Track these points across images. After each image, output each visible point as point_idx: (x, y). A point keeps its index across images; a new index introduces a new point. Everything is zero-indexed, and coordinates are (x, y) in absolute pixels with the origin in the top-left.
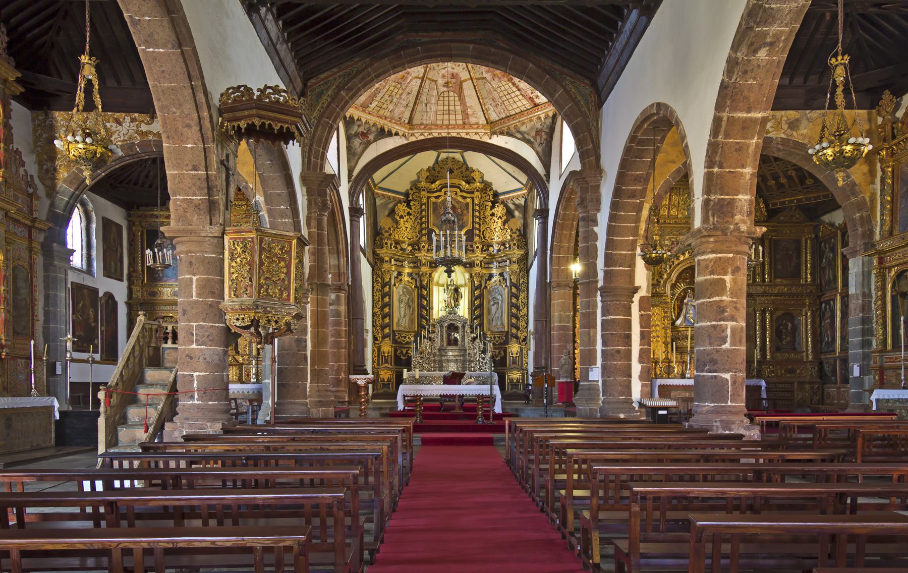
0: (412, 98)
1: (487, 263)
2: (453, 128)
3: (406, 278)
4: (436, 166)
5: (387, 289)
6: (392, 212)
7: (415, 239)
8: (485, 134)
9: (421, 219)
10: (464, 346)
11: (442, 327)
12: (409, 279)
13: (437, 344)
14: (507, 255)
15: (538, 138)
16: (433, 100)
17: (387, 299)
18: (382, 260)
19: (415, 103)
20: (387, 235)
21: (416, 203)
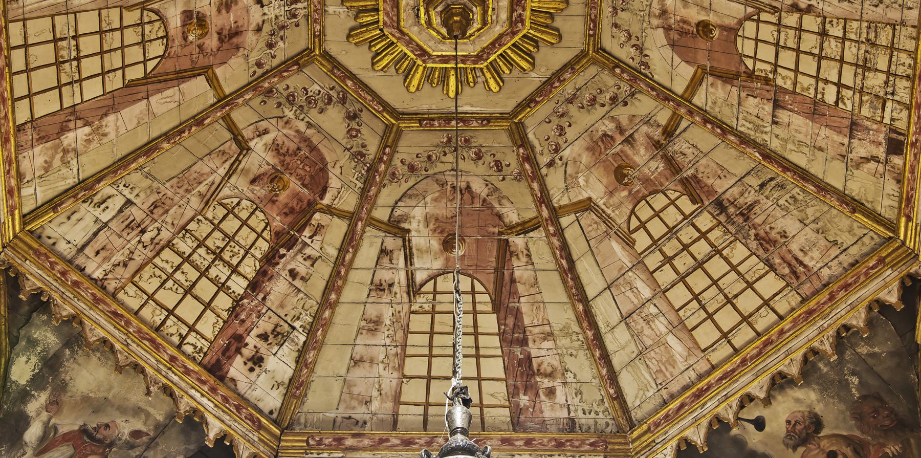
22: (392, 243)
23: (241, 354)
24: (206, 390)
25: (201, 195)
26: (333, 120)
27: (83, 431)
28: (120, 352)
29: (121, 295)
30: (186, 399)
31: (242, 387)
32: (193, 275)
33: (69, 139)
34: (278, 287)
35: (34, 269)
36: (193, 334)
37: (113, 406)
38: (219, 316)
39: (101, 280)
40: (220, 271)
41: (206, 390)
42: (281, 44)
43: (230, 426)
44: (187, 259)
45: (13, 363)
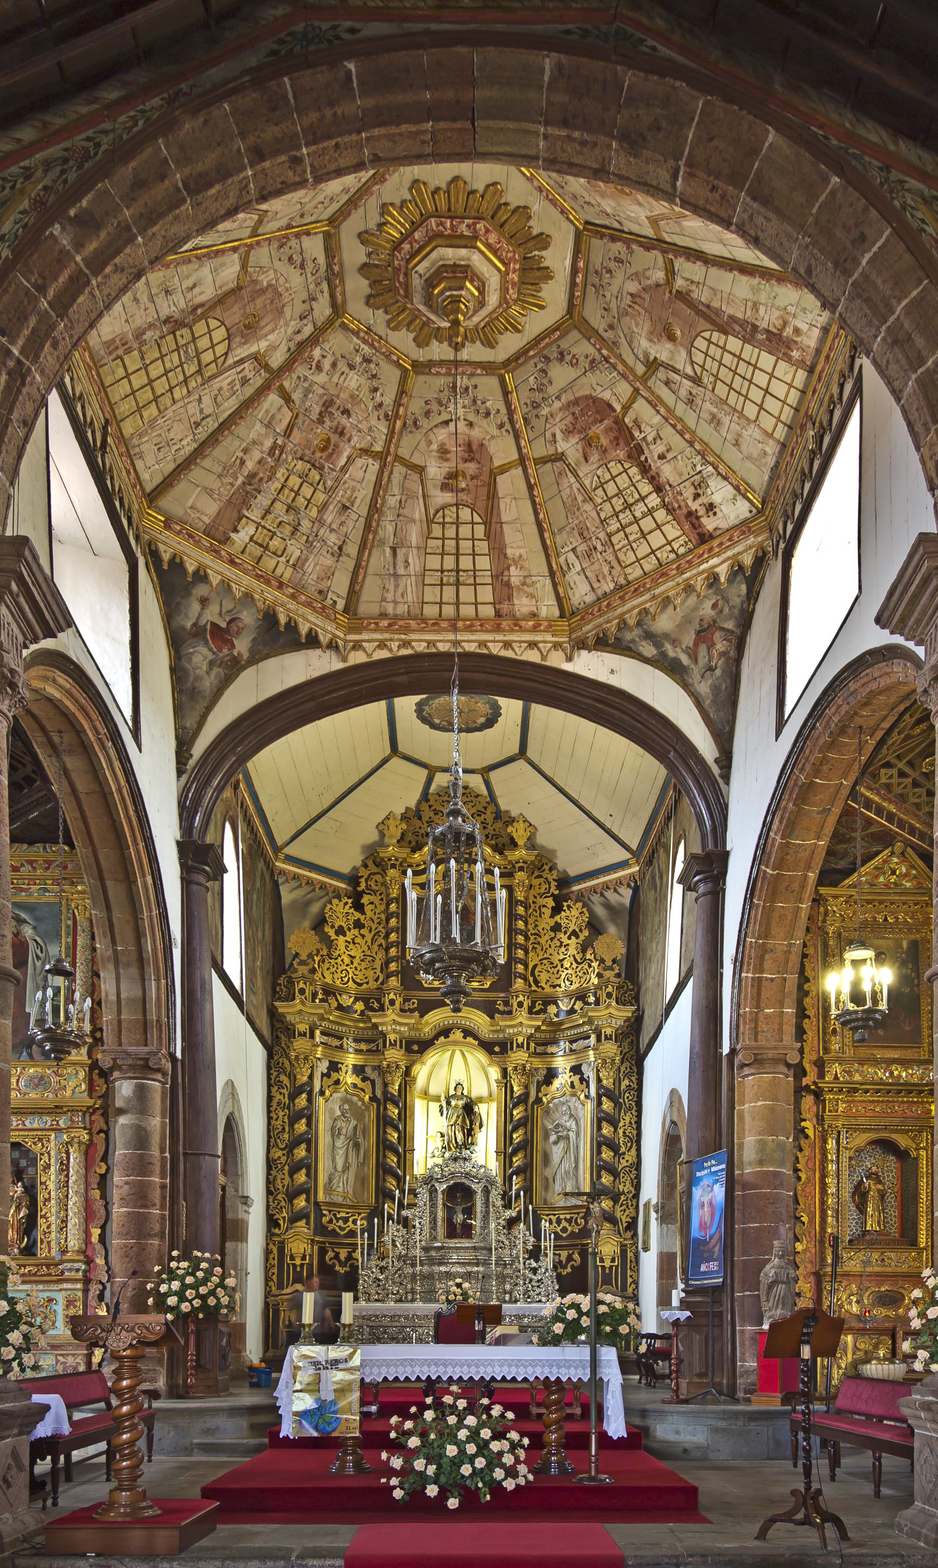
0: (354, 527)
1: (542, 1043)
2: (469, 629)
3: (350, 1079)
4: (425, 806)
5: (302, 1101)
6: (319, 923)
7: (373, 985)
8: (557, 646)
9: (387, 936)
10: (485, 1237)
11: (433, 1191)
12: (358, 1081)
13: (420, 1236)
14: (590, 1021)
15: (702, 651)
16: (414, 535)
17: (301, 1127)
18: (290, 1032)
19: (363, 546)
20: (303, 970)
21: (376, 899)
22: (662, 374)
25: (584, 501)
26: (561, 375)
27: (698, 633)
29: (630, 578)
31: (724, 525)
32: (635, 528)
33: (515, 581)
34: (667, 472)
40: (639, 509)
42: (488, 404)
44: (623, 528)
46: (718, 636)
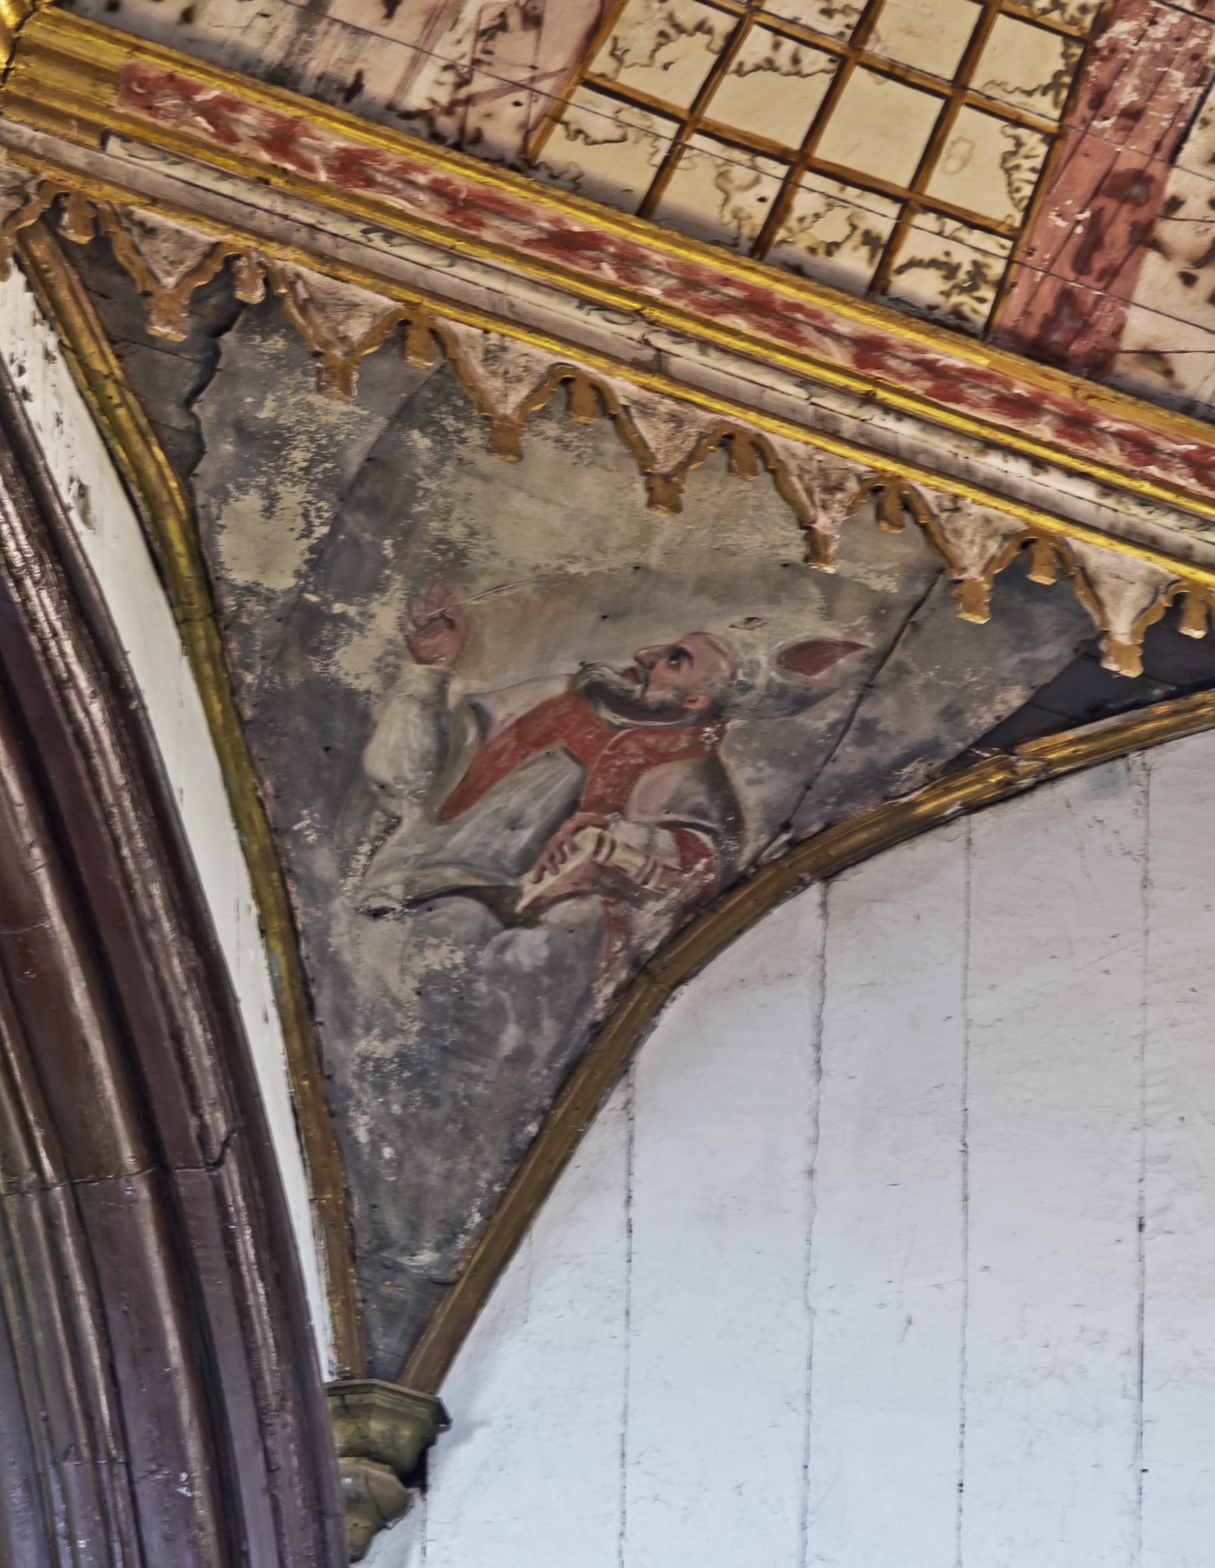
23: (1156, 245)
24: (1047, 434)
27: (591, 691)
28: (646, 410)
29: (557, 150)
30: (977, 505)
35: (154, 170)
36: (927, 221)
37: (675, 585)
38: (1017, 123)
39: (449, 110)
41: (1047, 434)
43: (1184, 556)
45: (215, 527)
46: (669, 782)
